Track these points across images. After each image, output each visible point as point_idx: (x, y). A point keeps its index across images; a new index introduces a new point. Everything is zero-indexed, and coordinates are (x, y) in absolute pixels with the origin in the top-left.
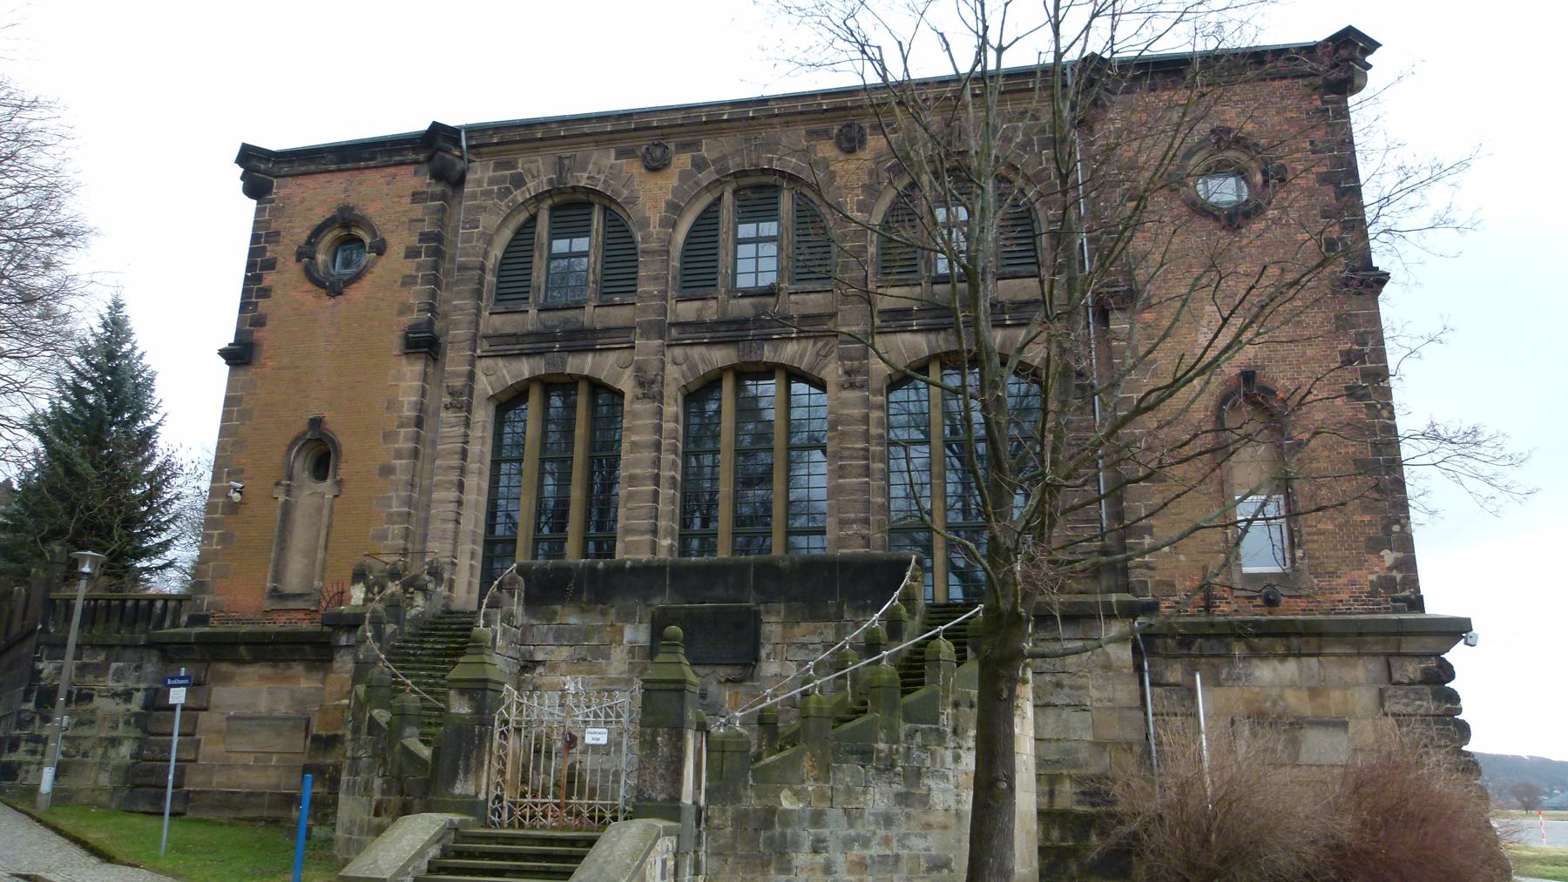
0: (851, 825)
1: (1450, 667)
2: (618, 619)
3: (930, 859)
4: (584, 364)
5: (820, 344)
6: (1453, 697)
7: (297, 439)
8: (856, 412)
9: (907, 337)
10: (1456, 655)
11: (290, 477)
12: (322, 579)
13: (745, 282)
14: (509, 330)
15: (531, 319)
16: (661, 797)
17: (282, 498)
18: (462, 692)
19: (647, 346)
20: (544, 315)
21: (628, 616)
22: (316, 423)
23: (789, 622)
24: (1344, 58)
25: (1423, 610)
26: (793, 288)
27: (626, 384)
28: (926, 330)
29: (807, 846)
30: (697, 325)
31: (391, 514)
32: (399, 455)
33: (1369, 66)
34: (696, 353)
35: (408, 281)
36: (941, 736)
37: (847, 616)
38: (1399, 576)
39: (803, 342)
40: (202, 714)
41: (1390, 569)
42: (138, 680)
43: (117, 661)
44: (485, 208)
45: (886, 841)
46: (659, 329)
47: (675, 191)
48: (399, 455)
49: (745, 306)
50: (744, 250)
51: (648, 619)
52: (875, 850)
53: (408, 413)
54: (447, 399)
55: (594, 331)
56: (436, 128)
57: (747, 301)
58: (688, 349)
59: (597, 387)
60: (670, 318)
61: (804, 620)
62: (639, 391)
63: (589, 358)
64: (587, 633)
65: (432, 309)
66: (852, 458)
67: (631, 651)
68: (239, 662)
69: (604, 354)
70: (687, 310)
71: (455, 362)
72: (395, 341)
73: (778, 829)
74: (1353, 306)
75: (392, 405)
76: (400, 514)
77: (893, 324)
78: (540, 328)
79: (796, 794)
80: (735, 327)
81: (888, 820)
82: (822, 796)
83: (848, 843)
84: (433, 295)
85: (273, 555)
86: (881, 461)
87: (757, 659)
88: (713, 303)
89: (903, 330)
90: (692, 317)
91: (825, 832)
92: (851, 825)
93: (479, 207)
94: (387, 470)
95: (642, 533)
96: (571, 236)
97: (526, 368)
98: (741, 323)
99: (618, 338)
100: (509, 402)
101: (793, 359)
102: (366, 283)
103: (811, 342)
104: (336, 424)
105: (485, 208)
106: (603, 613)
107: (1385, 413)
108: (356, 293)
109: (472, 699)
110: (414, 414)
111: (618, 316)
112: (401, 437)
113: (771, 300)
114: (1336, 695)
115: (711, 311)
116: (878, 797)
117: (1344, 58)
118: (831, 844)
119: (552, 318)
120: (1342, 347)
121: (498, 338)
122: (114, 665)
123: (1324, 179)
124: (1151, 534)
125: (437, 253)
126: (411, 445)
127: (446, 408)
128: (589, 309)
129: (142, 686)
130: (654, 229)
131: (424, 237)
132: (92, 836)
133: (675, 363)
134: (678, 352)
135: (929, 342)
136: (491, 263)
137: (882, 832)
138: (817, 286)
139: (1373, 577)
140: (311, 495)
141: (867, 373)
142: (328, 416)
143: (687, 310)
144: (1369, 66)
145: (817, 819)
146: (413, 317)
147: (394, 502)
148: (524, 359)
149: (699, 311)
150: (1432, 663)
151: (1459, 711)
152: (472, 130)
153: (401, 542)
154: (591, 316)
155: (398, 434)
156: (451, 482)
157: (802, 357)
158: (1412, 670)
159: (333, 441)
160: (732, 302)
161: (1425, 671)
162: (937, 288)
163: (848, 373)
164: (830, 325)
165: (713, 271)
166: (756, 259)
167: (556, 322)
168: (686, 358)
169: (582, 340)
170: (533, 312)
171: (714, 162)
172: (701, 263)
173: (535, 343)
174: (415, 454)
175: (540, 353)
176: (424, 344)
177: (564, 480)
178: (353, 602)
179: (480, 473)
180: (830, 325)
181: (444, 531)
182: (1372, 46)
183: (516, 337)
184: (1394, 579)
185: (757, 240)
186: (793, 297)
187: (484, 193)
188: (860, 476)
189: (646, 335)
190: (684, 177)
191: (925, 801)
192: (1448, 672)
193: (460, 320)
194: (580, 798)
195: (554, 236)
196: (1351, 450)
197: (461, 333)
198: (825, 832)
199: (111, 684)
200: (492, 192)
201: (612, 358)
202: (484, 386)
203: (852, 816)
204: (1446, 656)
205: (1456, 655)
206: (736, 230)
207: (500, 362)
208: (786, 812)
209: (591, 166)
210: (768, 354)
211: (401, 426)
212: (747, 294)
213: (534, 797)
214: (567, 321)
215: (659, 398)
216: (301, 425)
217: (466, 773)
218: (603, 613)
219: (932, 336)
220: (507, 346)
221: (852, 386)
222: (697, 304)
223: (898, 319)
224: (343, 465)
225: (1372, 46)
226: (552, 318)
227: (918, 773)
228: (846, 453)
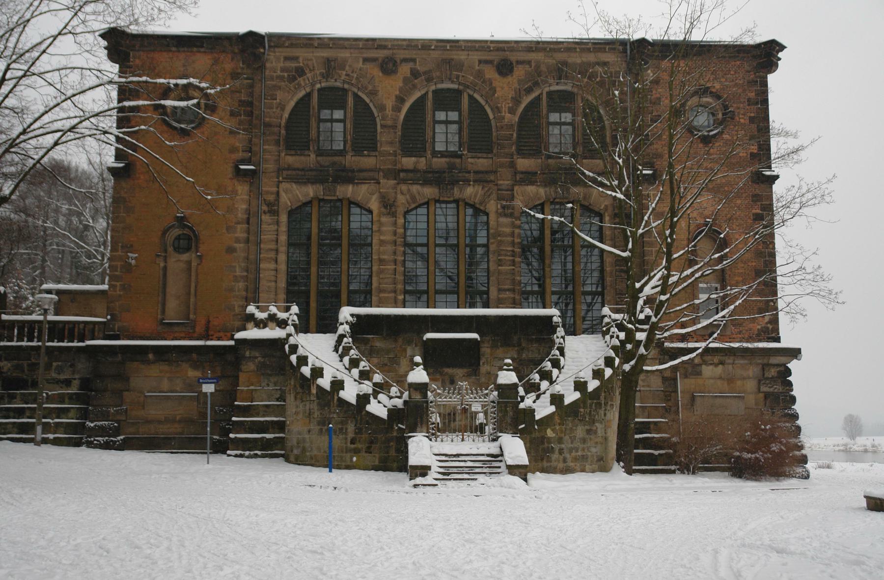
0: (572, 443)
1: (790, 370)
3: (597, 456)
6: (790, 384)
8: (508, 230)
10: (793, 365)
11: (166, 251)
12: (195, 314)
13: (440, 147)
14: (297, 165)
17: (162, 265)
20: (319, 158)
23: (494, 346)
24: (766, 55)
25: (778, 340)
29: (557, 452)
30: (415, 171)
31: (236, 276)
32: (238, 240)
33: (780, 59)
34: (415, 188)
36: (600, 404)
38: (770, 327)
40: (125, 393)
41: (767, 323)
42: (73, 374)
43: (56, 361)
44: (280, 88)
45: (583, 450)
47: (401, 90)
48: (238, 240)
49: (440, 163)
50: (439, 129)
52: (580, 453)
53: (241, 216)
54: (265, 208)
56: (251, 34)
57: (443, 160)
58: (410, 186)
60: (399, 166)
62: (383, 210)
64: (388, 352)
65: (250, 151)
66: (506, 255)
68: (148, 362)
70: (408, 162)
71: (268, 186)
73: (546, 445)
74: (758, 189)
76: (242, 277)
79: (552, 430)
81: (584, 441)
82: (562, 432)
83: (570, 451)
84: (250, 141)
85: (160, 299)
87: (479, 364)
88: (423, 159)
90: (411, 167)
91: (563, 446)
92: (572, 443)
93: (275, 86)
94: (231, 250)
95: (389, 292)
97: (310, 191)
105: (280, 88)
106: (396, 341)
107: (771, 246)
109: (421, 392)
110: (246, 216)
112: (239, 230)
113: (458, 161)
114: (739, 383)
115: (422, 163)
116: (580, 431)
117: (766, 55)
118: (565, 451)
119: (325, 161)
120: (754, 211)
122: (55, 364)
123: (752, 120)
125: (250, 114)
126: (245, 235)
127: (265, 212)
128: (348, 157)
129: (77, 376)
130: (389, 112)
131: (242, 103)
133: (402, 193)
134: (404, 187)
135: (546, 192)
136: (284, 122)
137: (582, 446)
138: (485, 155)
139: (759, 327)
140: (177, 262)
141: (513, 209)
144: (780, 59)
145: (560, 440)
147: (237, 269)
149: (417, 162)
150: (782, 369)
151: (792, 390)
152: (271, 36)
153: (244, 293)
156: (271, 258)
157: (475, 196)
158: (773, 372)
161: (779, 372)
162: (550, 161)
163: (503, 207)
164: (492, 178)
165: (424, 142)
166: (445, 134)
167: (327, 164)
169: (347, 176)
170: (313, 156)
171: (425, 73)
172: (414, 135)
173: (318, 176)
174: (247, 241)
181: (269, 287)
182: (782, 48)
184: (768, 328)
185: (447, 122)
187: (278, 77)
189: (386, 177)
190: (405, 80)
191: (596, 432)
192: (789, 372)
195: (321, 107)
196: (754, 264)
197: (270, 166)
198: (563, 446)
199: (54, 375)
200: (283, 77)
203: (573, 440)
204: (788, 365)
205: (793, 365)
206: (434, 115)
208: (549, 438)
209: (347, 68)
211: (238, 223)
212: (443, 154)
214: (334, 163)
215: (394, 215)
218: (396, 341)
221: (506, 215)
223: (528, 178)
224: (201, 245)
225: (782, 48)
226: (325, 161)
227: (594, 422)
228: (503, 253)
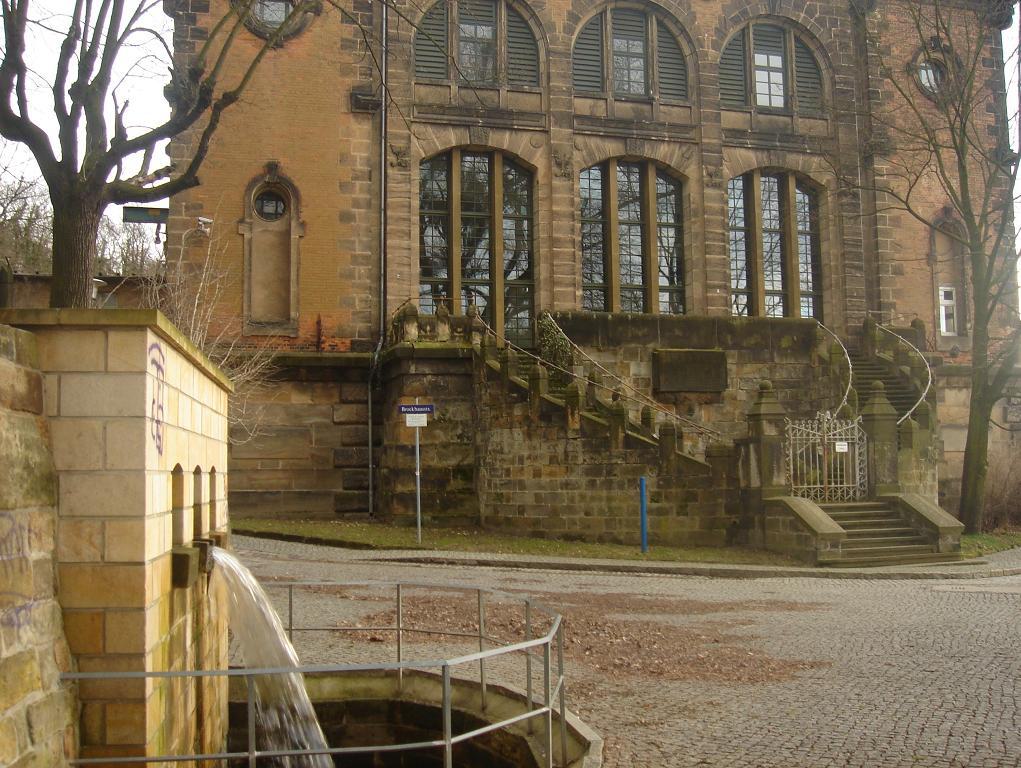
2: (625, 358)
4: (503, 140)
5: (684, 149)
7: (255, 181)
9: (743, 152)
15: (453, 93)
16: (889, 480)
18: (770, 422)
19: (560, 134)
20: (463, 92)
21: (633, 355)
22: (272, 167)
26: (663, 101)
27: (539, 161)
28: (755, 149)
30: (591, 119)
32: (356, 204)
34: (593, 142)
35: (347, 45)
37: (777, 360)
39: (672, 145)
46: (570, 119)
48: (356, 204)
49: (624, 109)
51: (646, 359)
55: (511, 113)
57: (629, 105)
58: (587, 139)
59: (511, 159)
61: (750, 362)
63: (507, 135)
66: (714, 240)
67: (636, 381)
69: (520, 134)
70: (583, 106)
72: (341, 100)
75: (344, 158)
77: (735, 141)
78: (462, 103)
80: (620, 125)
86: (557, 213)
89: (742, 146)
90: (587, 112)
96: (476, 23)
98: (626, 123)
99: (535, 122)
100: (441, 161)
101: (665, 156)
102: (307, 38)
103: (678, 146)
104: (290, 169)
108: (298, 48)
109: (777, 426)
111: (529, 102)
112: (357, 188)
115: (600, 110)
119: (470, 96)
121: (423, 107)
124: (895, 308)
130: (559, 33)
132: (349, 538)
135: (757, 158)
142: (283, 161)
143: (583, 106)
146: (356, 80)
148: (451, 129)
154: (505, 98)
155: (353, 185)
157: (672, 156)
159: (291, 185)
160: (618, 104)
168: (586, 145)
169: (501, 118)
170: (454, 88)
175: (467, 126)
176: (365, 104)
177: (447, 234)
178: (409, 337)
179: (553, 242)
180: (692, 134)
183: (443, 109)
186: (662, 107)
188: (720, 254)
193: (403, 85)
194: (802, 484)
201: (525, 138)
202: (418, 150)
207: (430, 129)
210: (647, 151)
211: (356, 178)
213: (809, 484)
216: (256, 168)
217: (779, 471)
218: (615, 354)
219: (759, 154)
220: (437, 115)
222: (590, 102)
226: (470, 96)
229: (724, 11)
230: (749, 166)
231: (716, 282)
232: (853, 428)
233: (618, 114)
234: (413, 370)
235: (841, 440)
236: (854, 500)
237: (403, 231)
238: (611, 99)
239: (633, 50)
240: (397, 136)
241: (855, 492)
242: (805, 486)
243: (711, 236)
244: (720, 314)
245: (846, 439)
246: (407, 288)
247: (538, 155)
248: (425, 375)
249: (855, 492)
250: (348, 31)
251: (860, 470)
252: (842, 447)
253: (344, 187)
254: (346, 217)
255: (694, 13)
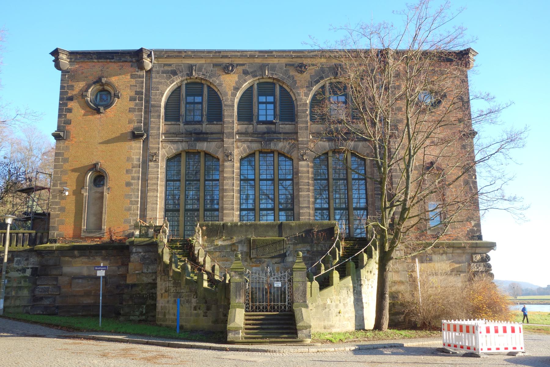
4: (203, 146)
35: (131, 110)
46: (342, 136)
55: (207, 133)
57: (264, 126)
66: (304, 185)
69: (211, 143)
75: (129, 159)
155: (132, 171)
160: (259, 126)
170: (182, 125)
213: (260, 302)
219: (330, 143)
229: (311, 78)
230: (325, 150)
231: (305, 205)
232: (285, 275)
233: (259, 130)
234: (134, 250)
235: (278, 281)
236: (285, 311)
237: (155, 189)
238: (255, 124)
239: (196, 101)
240: (153, 148)
241: (285, 307)
242: (258, 304)
243: (302, 184)
244: (307, 221)
245: (280, 281)
246: (158, 216)
247: (220, 152)
248: (140, 253)
249: (285, 307)
250: (132, 105)
251: (288, 296)
252: (278, 284)
253: (128, 171)
254: (128, 184)
255: (296, 81)
